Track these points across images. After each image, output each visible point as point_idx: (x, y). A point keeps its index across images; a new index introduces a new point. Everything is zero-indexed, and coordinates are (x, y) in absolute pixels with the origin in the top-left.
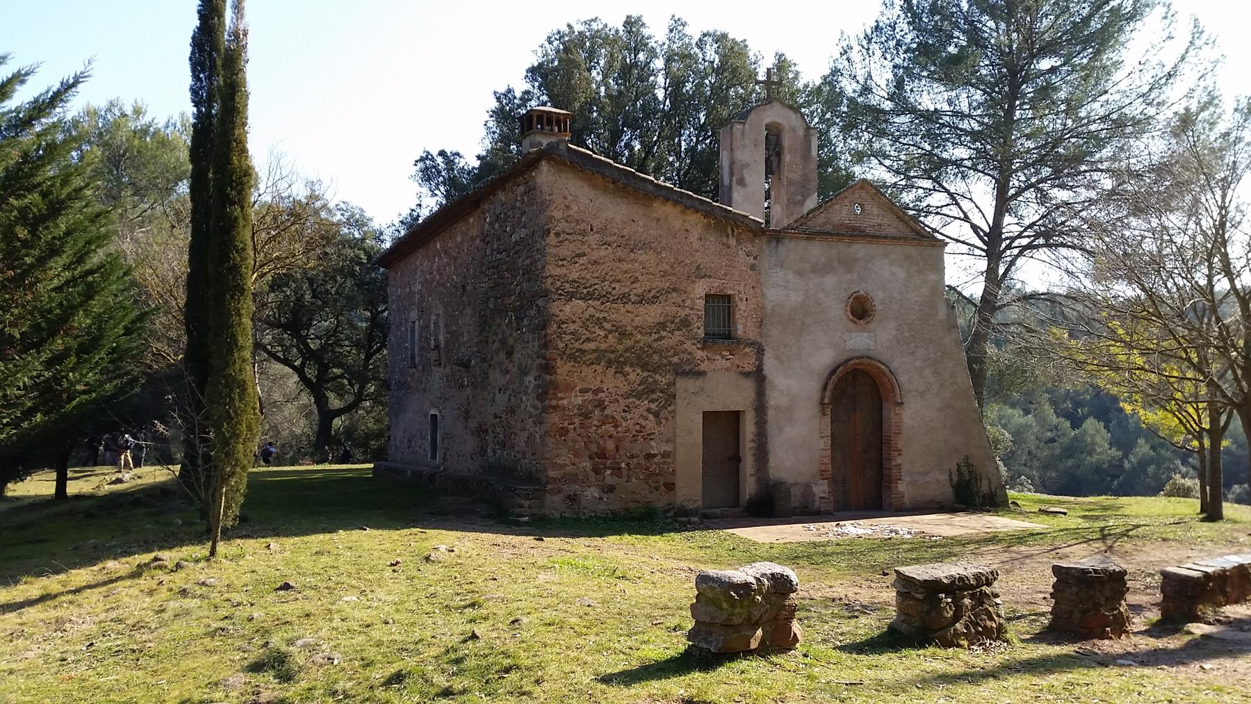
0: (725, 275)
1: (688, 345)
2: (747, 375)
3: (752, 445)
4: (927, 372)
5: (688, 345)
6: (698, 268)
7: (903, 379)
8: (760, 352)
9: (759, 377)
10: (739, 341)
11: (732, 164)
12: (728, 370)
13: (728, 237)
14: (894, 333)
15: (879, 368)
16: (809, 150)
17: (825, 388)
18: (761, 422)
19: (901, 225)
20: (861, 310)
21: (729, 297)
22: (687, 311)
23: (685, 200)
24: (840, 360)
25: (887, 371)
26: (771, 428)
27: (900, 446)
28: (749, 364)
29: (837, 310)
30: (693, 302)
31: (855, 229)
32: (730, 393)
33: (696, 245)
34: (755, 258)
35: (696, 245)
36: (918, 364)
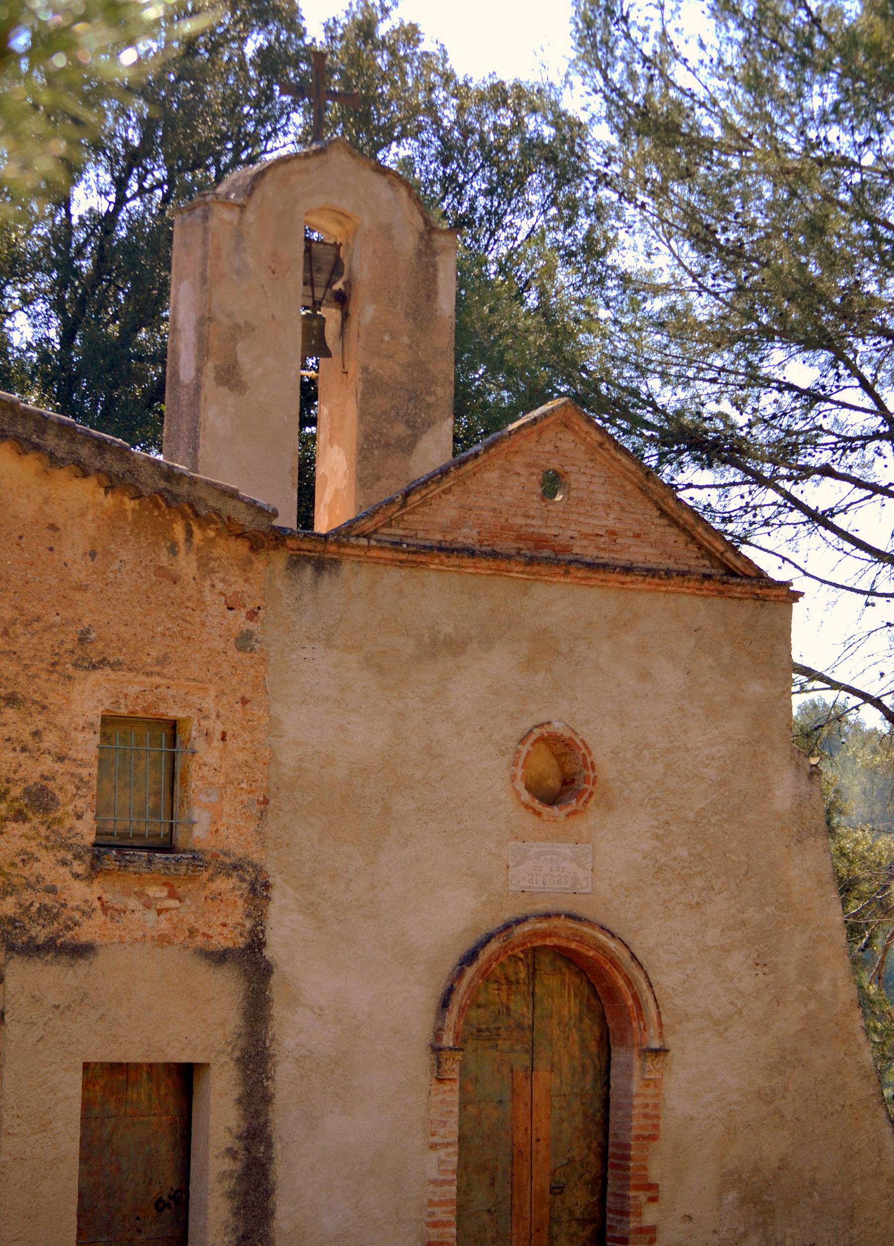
0: (162, 661)
1: (47, 866)
2: (219, 958)
3: (227, 1165)
4: (737, 961)
5: (47, 866)
6: (83, 638)
7: (667, 979)
8: (259, 891)
9: (252, 961)
10: (197, 860)
11: (204, 321)
12: (163, 940)
13: (173, 550)
14: (645, 846)
15: (600, 947)
16: (431, 295)
17: (445, 1003)
18: (256, 1099)
19: (672, 535)
20: (561, 780)
21: (173, 725)
22: (48, 764)
23: (50, 441)
24: (491, 921)
25: (623, 955)
26: (284, 1121)
27: (654, 1173)
28: (226, 927)
29: (491, 778)
30: (66, 737)
31: (540, 542)
32: (174, 1013)
33: (80, 571)
34: (252, 615)
35: (80, 571)
36: (712, 937)
